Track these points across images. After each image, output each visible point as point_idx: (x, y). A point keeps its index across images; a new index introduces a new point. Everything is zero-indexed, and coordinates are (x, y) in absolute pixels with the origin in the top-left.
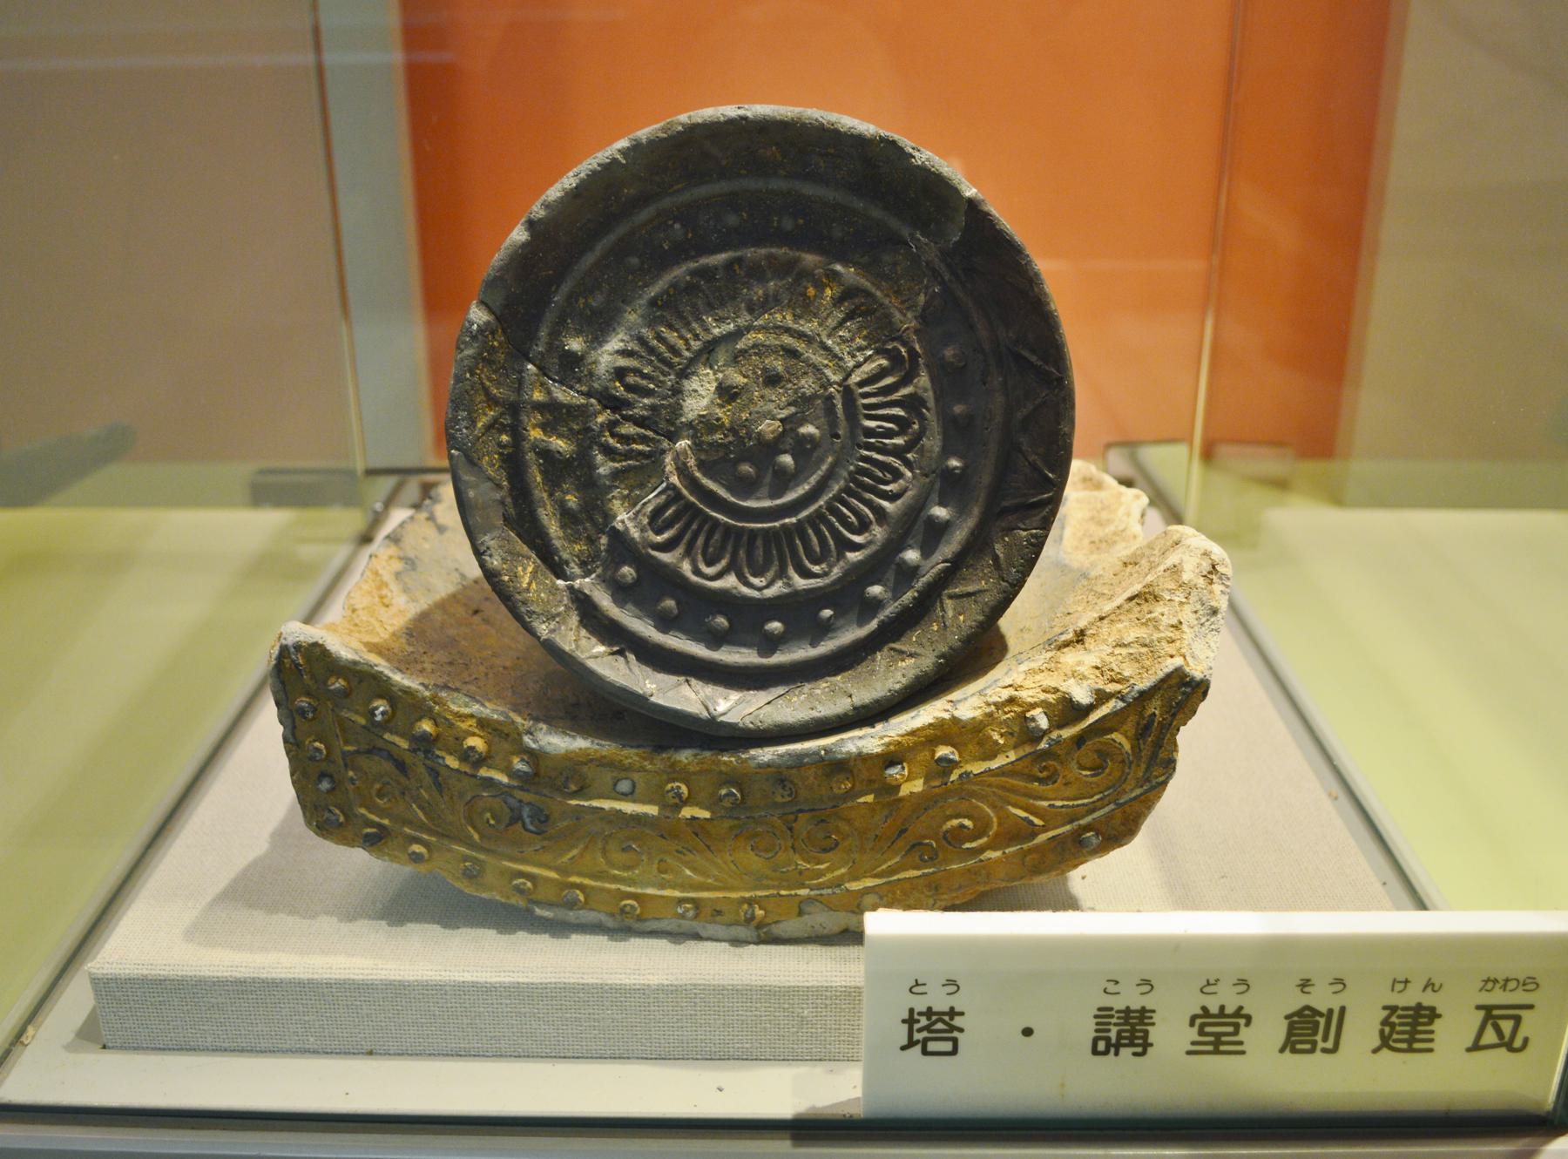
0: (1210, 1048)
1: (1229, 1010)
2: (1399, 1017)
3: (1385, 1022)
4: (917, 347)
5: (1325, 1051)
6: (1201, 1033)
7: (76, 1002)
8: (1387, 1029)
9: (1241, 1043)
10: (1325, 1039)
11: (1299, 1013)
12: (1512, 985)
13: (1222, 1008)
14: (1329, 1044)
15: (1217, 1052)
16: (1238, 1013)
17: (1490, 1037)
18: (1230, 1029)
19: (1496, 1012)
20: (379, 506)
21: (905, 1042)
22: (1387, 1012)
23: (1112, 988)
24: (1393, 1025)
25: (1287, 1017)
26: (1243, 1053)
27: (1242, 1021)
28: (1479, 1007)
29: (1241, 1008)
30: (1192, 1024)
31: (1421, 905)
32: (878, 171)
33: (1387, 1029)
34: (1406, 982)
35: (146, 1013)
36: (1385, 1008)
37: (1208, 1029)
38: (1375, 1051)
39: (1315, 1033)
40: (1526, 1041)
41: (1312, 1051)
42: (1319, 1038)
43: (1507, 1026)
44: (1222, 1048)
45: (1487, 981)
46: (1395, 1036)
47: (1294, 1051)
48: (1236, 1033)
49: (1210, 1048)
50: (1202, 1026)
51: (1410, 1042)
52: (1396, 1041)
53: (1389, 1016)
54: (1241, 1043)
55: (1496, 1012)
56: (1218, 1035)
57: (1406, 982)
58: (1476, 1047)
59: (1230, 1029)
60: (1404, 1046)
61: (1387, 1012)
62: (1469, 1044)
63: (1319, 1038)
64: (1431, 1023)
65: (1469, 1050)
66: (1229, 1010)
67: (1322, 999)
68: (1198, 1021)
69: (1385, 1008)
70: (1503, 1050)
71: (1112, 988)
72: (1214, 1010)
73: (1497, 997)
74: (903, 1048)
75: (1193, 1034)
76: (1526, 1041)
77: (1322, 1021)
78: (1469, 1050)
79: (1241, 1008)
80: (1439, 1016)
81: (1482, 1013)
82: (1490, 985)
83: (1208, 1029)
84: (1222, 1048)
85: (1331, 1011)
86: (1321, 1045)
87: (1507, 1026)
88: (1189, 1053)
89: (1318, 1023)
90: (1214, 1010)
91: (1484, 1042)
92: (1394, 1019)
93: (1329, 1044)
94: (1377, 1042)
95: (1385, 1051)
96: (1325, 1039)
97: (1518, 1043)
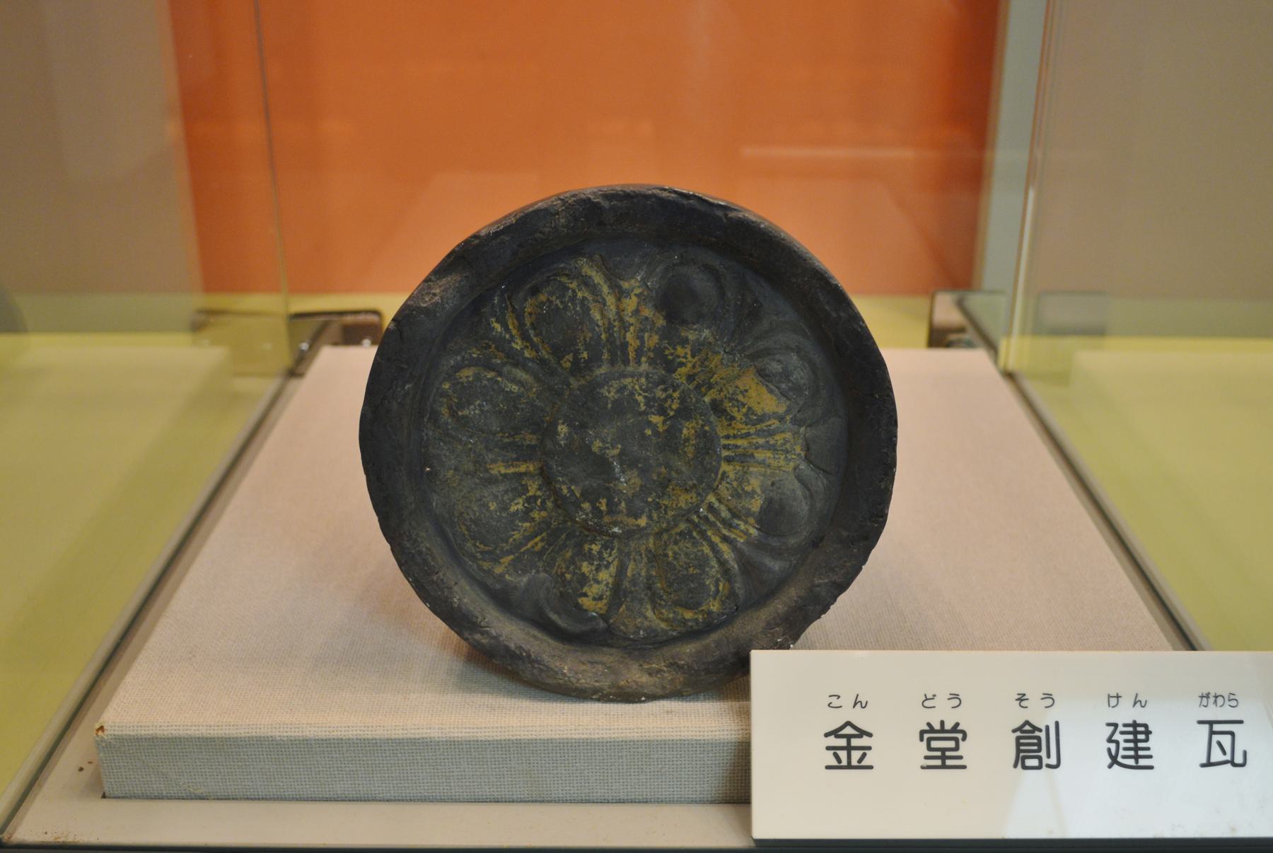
1: (948, 726)
3: (1110, 740)
5: (1049, 766)
6: (929, 748)
9: (960, 758)
12: (1220, 701)
13: (942, 723)
15: (944, 766)
16: (955, 728)
17: (1217, 756)
18: (951, 744)
19: (1217, 728)
20: (305, 346)
21: (1204, 761)
23: (835, 702)
26: (964, 767)
27: (960, 736)
28: (1201, 722)
29: (957, 724)
31: (1188, 642)
33: (1113, 746)
34: (1118, 697)
36: (929, 724)
37: (934, 744)
39: (1039, 750)
41: (1040, 767)
42: (1043, 753)
43: (1225, 741)
45: (1202, 697)
47: (1025, 767)
48: (957, 748)
50: (929, 740)
51: (1137, 757)
54: (960, 758)
55: (1217, 728)
56: (943, 750)
57: (1118, 697)
58: (1209, 764)
59: (951, 744)
63: (1043, 753)
65: (1203, 766)
66: (948, 726)
67: (943, 714)
68: (926, 736)
71: (835, 702)
73: (1212, 713)
74: (1203, 766)
77: (1043, 735)
79: (957, 724)
81: (1207, 726)
83: (934, 744)
84: (949, 762)
86: (1045, 761)
89: (1039, 738)
93: (1053, 761)
97: (1239, 760)
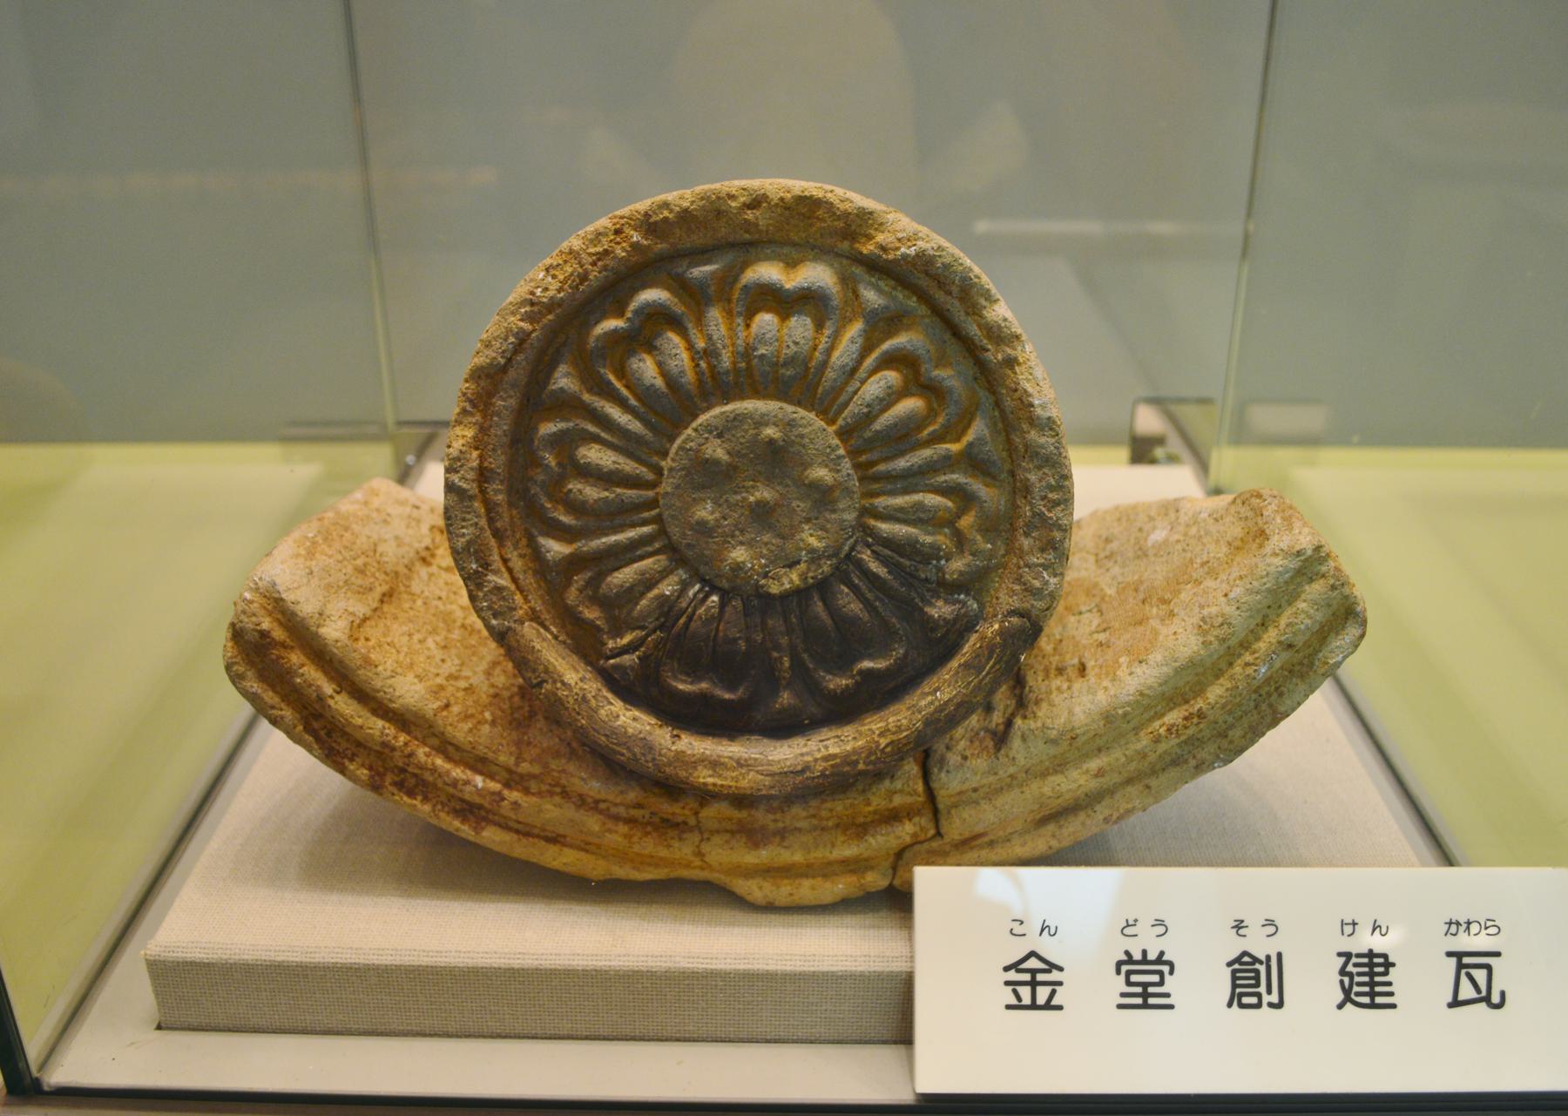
0: (1139, 1001)
1: (1152, 956)
2: (1355, 965)
3: (1343, 972)
4: (644, 602)
5: (1271, 1005)
6: (1129, 983)
7: (130, 985)
8: (1346, 980)
9: (1167, 995)
10: (1269, 992)
11: (1238, 960)
12: (1474, 928)
13: (1144, 952)
14: (1274, 998)
15: (1145, 1006)
16: (1160, 960)
17: (1467, 991)
18: (1156, 978)
19: (1466, 960)
22: (1343, 959)
24: (1351, 975)
25: (1229, 964)
27: (1166, 969)
28: (1450, 954)
29: (1162, 953)
30: (1118, 972)
32: (807, 207)
33: (1346, 980)
35: (200, 995)
37: (1134, 978)
38: (1340, 1006)
39: (1258, 985)
40: (1503, 994)
41: (1258, 1006)
42: (1262, 989)
43: (1481, 976)
44: (1151, 1001)
46: (1356, 989)
48: (1161, 983)
49: (1139, 1001)
50: (1129, 973)
52: (1358, 994)
53: (1346, 964)
54: (1167, 995)
55: (1466, 960)
56: (1145, 985)
57: (1354, 924)
58: (1455, 1003)
59: (1156, 978)
60: (1366, 1000)
61: (1343, 959)
62: (1450, 999)
63: (1262, 989)
64: (1386, 973)
65: (1450, 1006)
66: (1152, 956)
68: (1124, 968)
69: (1340, 954)
70: (1483, 1005)
71: (1018, 929)
72: (1137, 956)
73: (1465, 942)
75: (1119, 984)
76: (1503, 994)
77: (1262, 969)
78: (1450, 1006)
80: (1393, 965)
81: (1453, 960)
82: (1454, 928)
83: (1134, 978)
84: (1151, 1001)
85: (1268, 958)
86: (1266, 999)
87: (1481, 976)
88: (1120, 1006)
89: (1257, 972)
90: (1137, 956)
91: (1461, 997)
92: (1350, 968)
93: (1274, 998)
94: (1340, 996)
95: (1349, 1006)
96: (1269, 992)
97: (1496, 999)
